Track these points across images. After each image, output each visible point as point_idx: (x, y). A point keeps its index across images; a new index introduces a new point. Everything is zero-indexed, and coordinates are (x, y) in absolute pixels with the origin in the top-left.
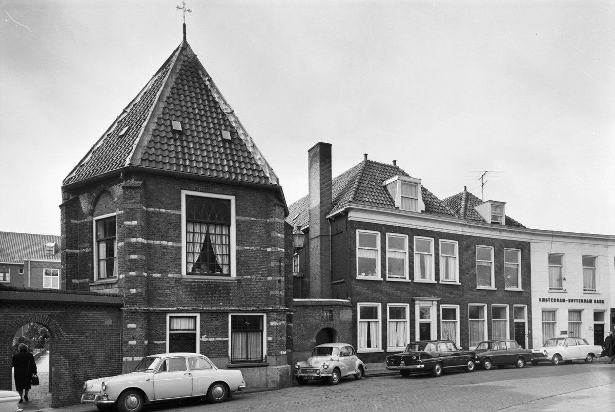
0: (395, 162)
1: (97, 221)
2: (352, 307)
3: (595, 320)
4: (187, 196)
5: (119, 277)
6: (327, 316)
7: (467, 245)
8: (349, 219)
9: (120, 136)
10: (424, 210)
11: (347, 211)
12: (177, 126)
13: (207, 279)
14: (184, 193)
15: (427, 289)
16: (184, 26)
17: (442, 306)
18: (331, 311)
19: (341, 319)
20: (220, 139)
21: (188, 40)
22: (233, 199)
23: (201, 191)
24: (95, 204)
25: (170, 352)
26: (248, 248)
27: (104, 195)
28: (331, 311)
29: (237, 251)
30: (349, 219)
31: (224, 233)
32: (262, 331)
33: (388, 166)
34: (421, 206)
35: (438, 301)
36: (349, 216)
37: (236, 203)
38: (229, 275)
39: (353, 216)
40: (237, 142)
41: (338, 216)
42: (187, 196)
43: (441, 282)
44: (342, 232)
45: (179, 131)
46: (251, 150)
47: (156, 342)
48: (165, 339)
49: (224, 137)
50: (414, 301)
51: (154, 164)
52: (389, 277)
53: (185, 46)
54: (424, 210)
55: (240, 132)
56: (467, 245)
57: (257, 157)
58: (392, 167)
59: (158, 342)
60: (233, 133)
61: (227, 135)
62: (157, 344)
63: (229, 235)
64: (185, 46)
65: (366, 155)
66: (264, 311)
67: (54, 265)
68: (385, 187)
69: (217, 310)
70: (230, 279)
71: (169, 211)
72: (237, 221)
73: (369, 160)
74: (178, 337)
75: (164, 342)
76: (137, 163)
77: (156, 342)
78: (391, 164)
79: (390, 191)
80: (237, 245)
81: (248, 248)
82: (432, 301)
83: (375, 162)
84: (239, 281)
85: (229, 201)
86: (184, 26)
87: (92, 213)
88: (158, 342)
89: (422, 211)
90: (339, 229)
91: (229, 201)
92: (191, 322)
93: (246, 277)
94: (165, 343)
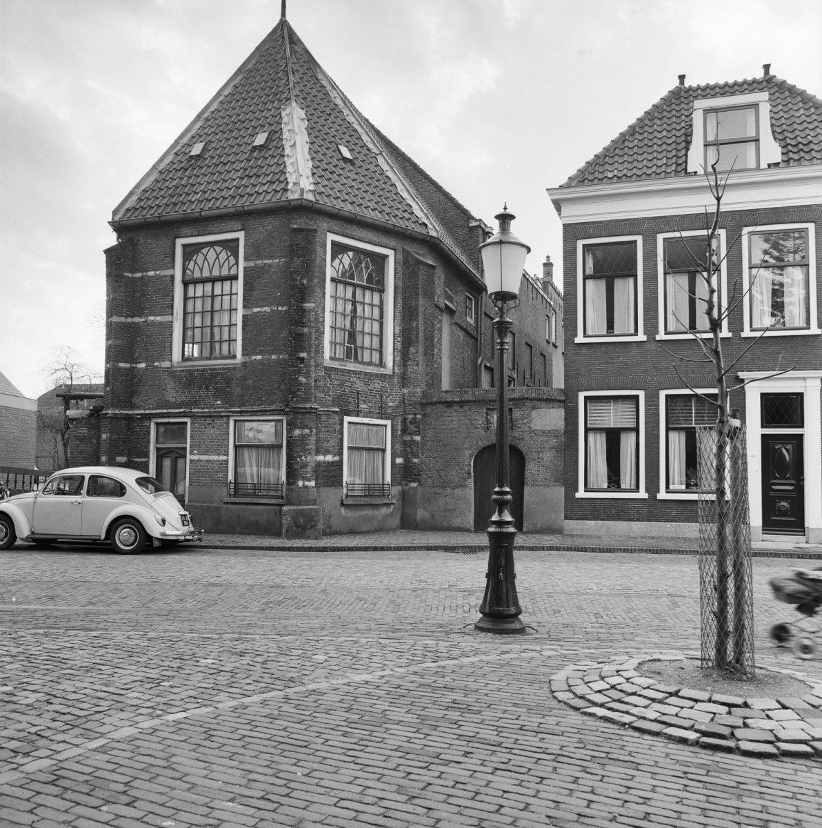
3: (801, 437)
4: (237, 240)
21: (288, 18)
23: (198, 235)
25: (765, 438)
26: (258, 309)
42: (237, 240)
47: (135, 460)
48: (147, 455)
53: (283, 25)
54: (778, 158)
59: (139, 460)
62: (137, 462)
64: (283, 25)
66: (192, 416)
69: (209, 412)
71: (158, 272)
75: (224, 458)
77: (135, 460)
81: (258, 309)
82: (804, 379)
84: (244, 364)
85: (184, 246)
88: (139, 460)
92: (629, 407)
93: (254, 357)
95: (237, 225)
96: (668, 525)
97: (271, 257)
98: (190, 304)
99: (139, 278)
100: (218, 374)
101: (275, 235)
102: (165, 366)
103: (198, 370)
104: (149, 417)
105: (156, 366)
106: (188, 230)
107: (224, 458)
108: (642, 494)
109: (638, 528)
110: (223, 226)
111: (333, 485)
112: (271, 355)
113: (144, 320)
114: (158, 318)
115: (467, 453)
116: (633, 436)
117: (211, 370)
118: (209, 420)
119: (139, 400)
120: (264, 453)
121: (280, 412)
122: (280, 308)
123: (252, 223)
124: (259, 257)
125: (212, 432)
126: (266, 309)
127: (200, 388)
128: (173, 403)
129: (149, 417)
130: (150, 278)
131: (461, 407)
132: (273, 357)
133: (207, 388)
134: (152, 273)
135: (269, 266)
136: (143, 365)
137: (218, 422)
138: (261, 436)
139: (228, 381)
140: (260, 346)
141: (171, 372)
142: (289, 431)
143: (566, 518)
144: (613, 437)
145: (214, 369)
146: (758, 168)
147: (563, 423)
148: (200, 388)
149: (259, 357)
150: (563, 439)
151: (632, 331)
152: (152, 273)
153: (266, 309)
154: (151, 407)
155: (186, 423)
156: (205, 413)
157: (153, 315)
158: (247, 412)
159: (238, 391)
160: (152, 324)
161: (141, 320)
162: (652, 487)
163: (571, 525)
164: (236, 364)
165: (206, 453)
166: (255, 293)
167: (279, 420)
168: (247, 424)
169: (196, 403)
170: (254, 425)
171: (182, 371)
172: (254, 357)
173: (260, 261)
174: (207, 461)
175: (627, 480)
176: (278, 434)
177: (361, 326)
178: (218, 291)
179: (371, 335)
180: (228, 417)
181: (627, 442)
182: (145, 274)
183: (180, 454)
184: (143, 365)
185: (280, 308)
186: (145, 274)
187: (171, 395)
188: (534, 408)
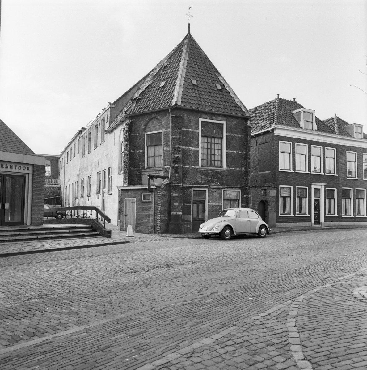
0: (295, 99)
1: (147, 135)
2: (276, 188)
4: (202, 122)
5: (164, 167)
6: (263, 193)
7: (341, 151)
8: (275, 134)
9: (160, 87)
10: (316, 129)
11: (273, 130)
12: (195, 82)
13: (212, 169)
14: (201, 120)
15: (318, 178)
16: (189, 25)
17: (326, 188)
18: (265, 190)
19: (271, 196)
20: (216, 89)
22: (224, 123)
24: (146, 125)
26: (233, 151)
27: (153, 120)
28: (265, 190)
29: (226, 153)
30: (275, 134)
31: (216, 142)
32: (351, 198)
33: (291, 101)
34: (315, 127)
35: (325, 186)
36: (275, 132)
37: (226, 125)
38: (221, 167)
39: (277, 133)
40: (224, 90)
41: (267, 132)
42: (202, 122)
43: (296, 172)
44: (269, 142)
45: (196, 85)
46: (233, 96)
49: (218, 88)
50: (311, 185)
51: (201, 106)
52: (280, 169)
54: (316, 129)
55: (226, 86)
56: (341, 151)
57: (237, 100)
58: (293, 102)
59: (187, 205)
60: (222, 85)
61: (219, 87)
62: (187, 206)
63: (222, 144)
65: (278, 95)
67: (341, 167)
68: (292, 114)
70: (223, 169)
71: (193, 130)
72: (227, 136)
73: (280, 98)
74: (196, 202)
75: (190, 205)
76: (179, 104)
78: (292, 100)
79: (296, 118)
80: (227, 149)
81: (233, 151)
82: (321, 185)
83: (285, 99)
85: (223, 124)
86: (189, 25)
87: (144, 130)
88: (187, 205)
89: (316, 130)
90: (266, 140)
91: (223, 124)
93: (231, 168)
94: (191, 205)
95: (224, 119)
96: (298, 223)
97: (236, 134)
98: (220, 148)
99: (185, 130)
100: (217, 173)
101: (237, 126)
102: (197, 168)
103: (210, 171)
104: (191, 187)
105: (193, 167)
106: (205, 116)
107: (209, 204)
108: (292, 215)
109: (337, 223)
110: (218, 118)
111: (189, 214)
112: (237, 168)
113: (187, 148)
114: (194, 148)
115: (257, 203)
116: (304, 199)
117: (215, 171)
118: (215, 190)
119: (186, 180)
120: (232, 202)
121: (239, 188)
122: (240, 152)
123: (229, 119)
124: (232, 133)
125: (217, 194)
126: (235, 151)
127: (211, 177)
128: (200, 183)
129: (191, 187)
130: (189, 131)
131: (256, 188)
132: (238, 169)
133: (214, 178)
134: (190, 130)
135: (236, 136)
136: (187, 166)
137: (219, 191)
138: (231, 197)
139: (222, 176)
140: (233, 165)
141: (199, 170)
142: (242, 195)
143: (277, 223)
144: (285, 198)
145: (216, 171)
146: (361, 138)
147: (276, 194)
148: (211, 177)
149: (233, 168)
150: (276, 198)
151: (289, 169)
152: (190, 130)
153: (235, 152)
154: (191, 183)
155: (205, 191)
156: (215, 187)
157: (191, 147)
158: (229, 188)
159: (225, 180)
160: (191, 150)
161: (186, 148)
162: (294, 213)
163: (279, 225)
164: (224, 170)
165: (214, 202)
166: (231, 145)
167: (238, 191)
168: (227, 192)
169: (209, 183)
170: (229, 192)
171: (204, 170)
172: (231, 168)
173: (232, 134)
174: (215, 205)
175: (332, 212)
176: (238, 196)
177: (208, 156)
178: (213, 141)
179: (218, 161)
180: (222, 189)
181: (288, 199)
182: (187, 129)
183: (203, 202)
184: (187, 166)
185: (240, 152)
186: (187, 129)
187: (200, 180)
188: (271, 189)
